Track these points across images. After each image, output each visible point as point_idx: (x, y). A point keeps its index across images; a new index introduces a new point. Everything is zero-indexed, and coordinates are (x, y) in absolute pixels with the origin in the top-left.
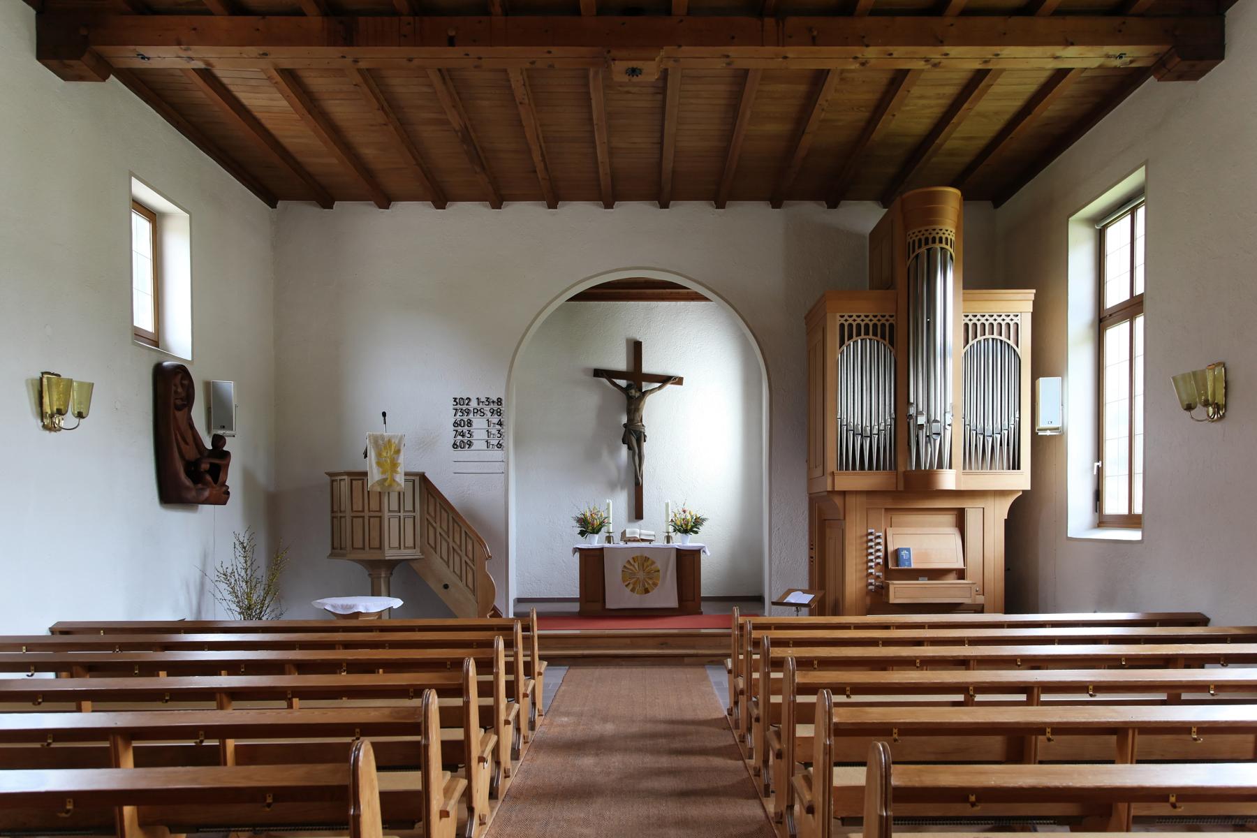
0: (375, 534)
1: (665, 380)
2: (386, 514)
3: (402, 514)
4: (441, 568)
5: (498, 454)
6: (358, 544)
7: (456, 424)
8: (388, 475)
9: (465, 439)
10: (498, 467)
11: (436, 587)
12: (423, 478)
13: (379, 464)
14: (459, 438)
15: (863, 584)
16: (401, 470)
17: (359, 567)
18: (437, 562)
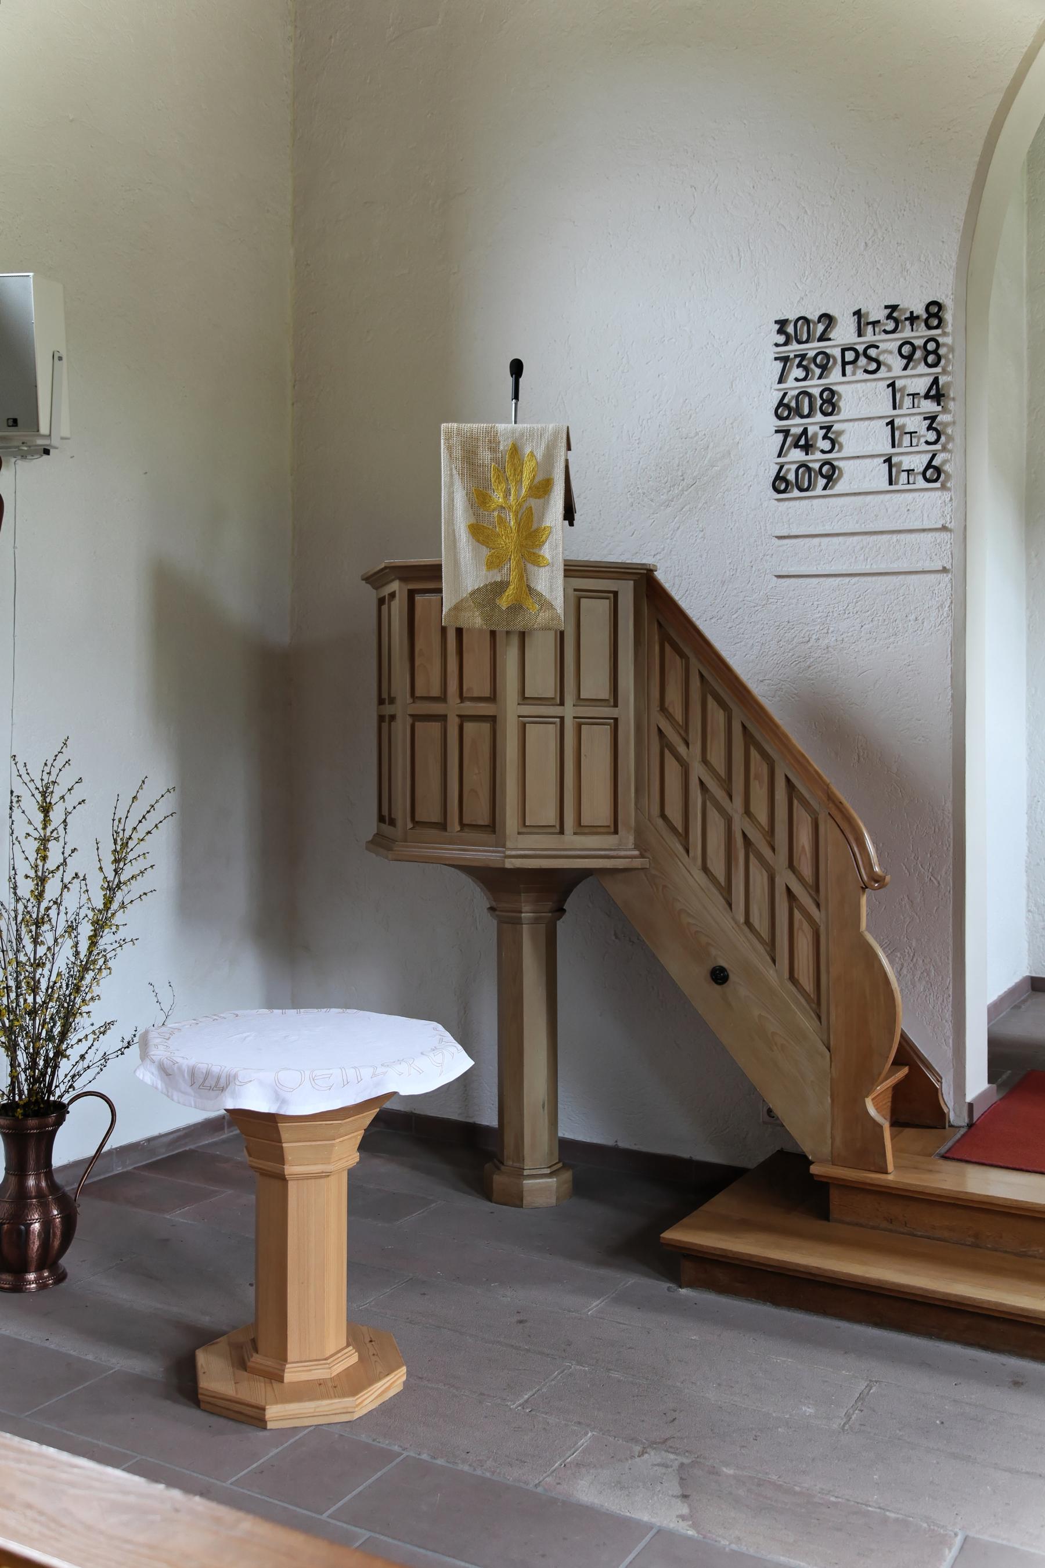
0: (477, 777)
1: (246, 1083)
2: (512, 709)
3: (569, 711)
4: (707, 909)
5: (928, 505)
6: (429, 812)
7: (784, 409)
8: (509, 572)
9: (815, 459)
10: (929, 550)
11: (685, 973)
12: (646, 584)
13: (479, 532)
14: (797, 455)
16: (558, 545)
17: (464, 878)
18: (691, 886)
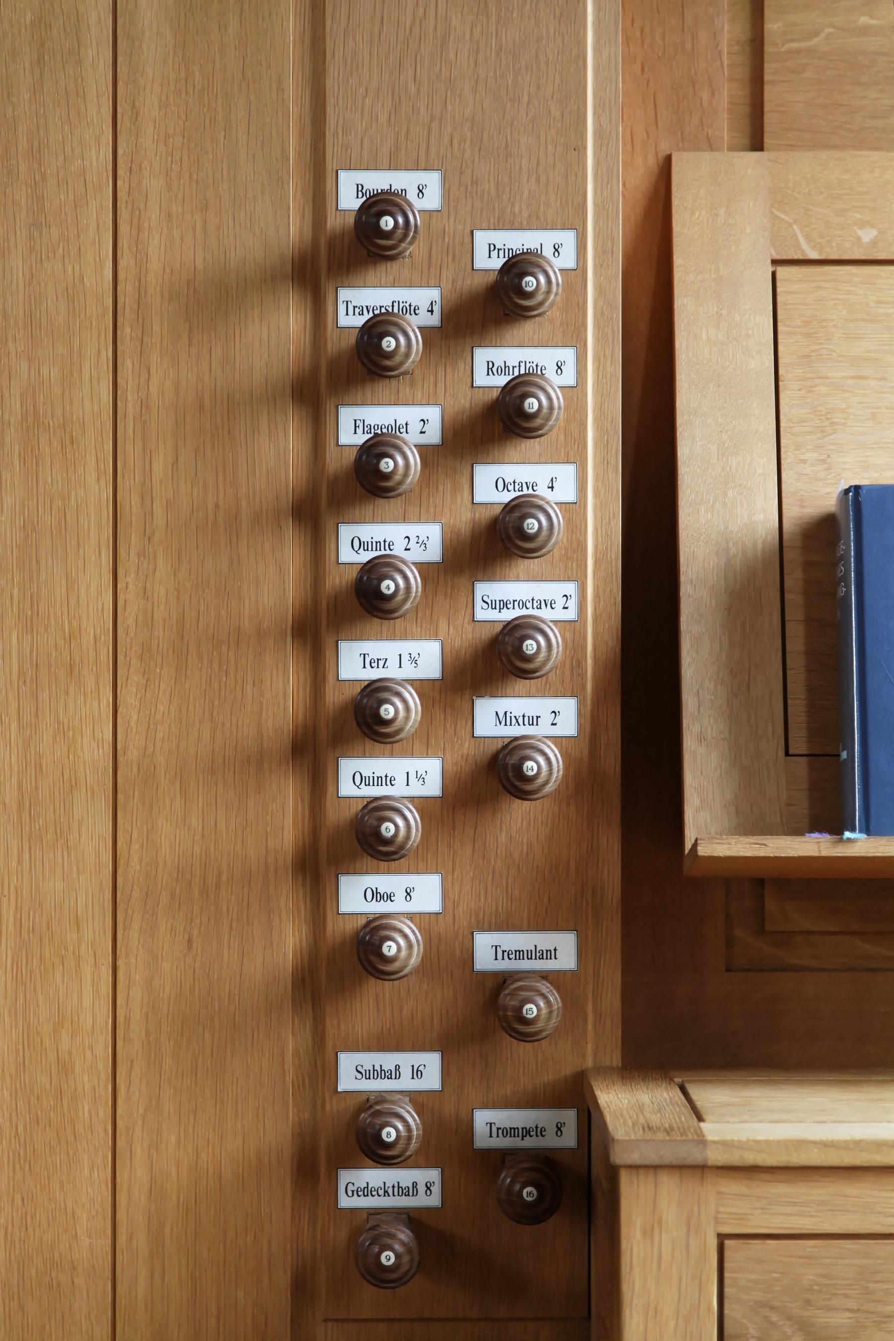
15: (257, 1123)
